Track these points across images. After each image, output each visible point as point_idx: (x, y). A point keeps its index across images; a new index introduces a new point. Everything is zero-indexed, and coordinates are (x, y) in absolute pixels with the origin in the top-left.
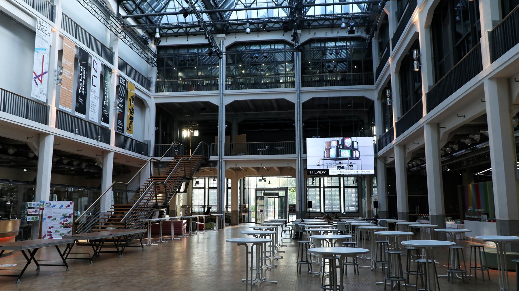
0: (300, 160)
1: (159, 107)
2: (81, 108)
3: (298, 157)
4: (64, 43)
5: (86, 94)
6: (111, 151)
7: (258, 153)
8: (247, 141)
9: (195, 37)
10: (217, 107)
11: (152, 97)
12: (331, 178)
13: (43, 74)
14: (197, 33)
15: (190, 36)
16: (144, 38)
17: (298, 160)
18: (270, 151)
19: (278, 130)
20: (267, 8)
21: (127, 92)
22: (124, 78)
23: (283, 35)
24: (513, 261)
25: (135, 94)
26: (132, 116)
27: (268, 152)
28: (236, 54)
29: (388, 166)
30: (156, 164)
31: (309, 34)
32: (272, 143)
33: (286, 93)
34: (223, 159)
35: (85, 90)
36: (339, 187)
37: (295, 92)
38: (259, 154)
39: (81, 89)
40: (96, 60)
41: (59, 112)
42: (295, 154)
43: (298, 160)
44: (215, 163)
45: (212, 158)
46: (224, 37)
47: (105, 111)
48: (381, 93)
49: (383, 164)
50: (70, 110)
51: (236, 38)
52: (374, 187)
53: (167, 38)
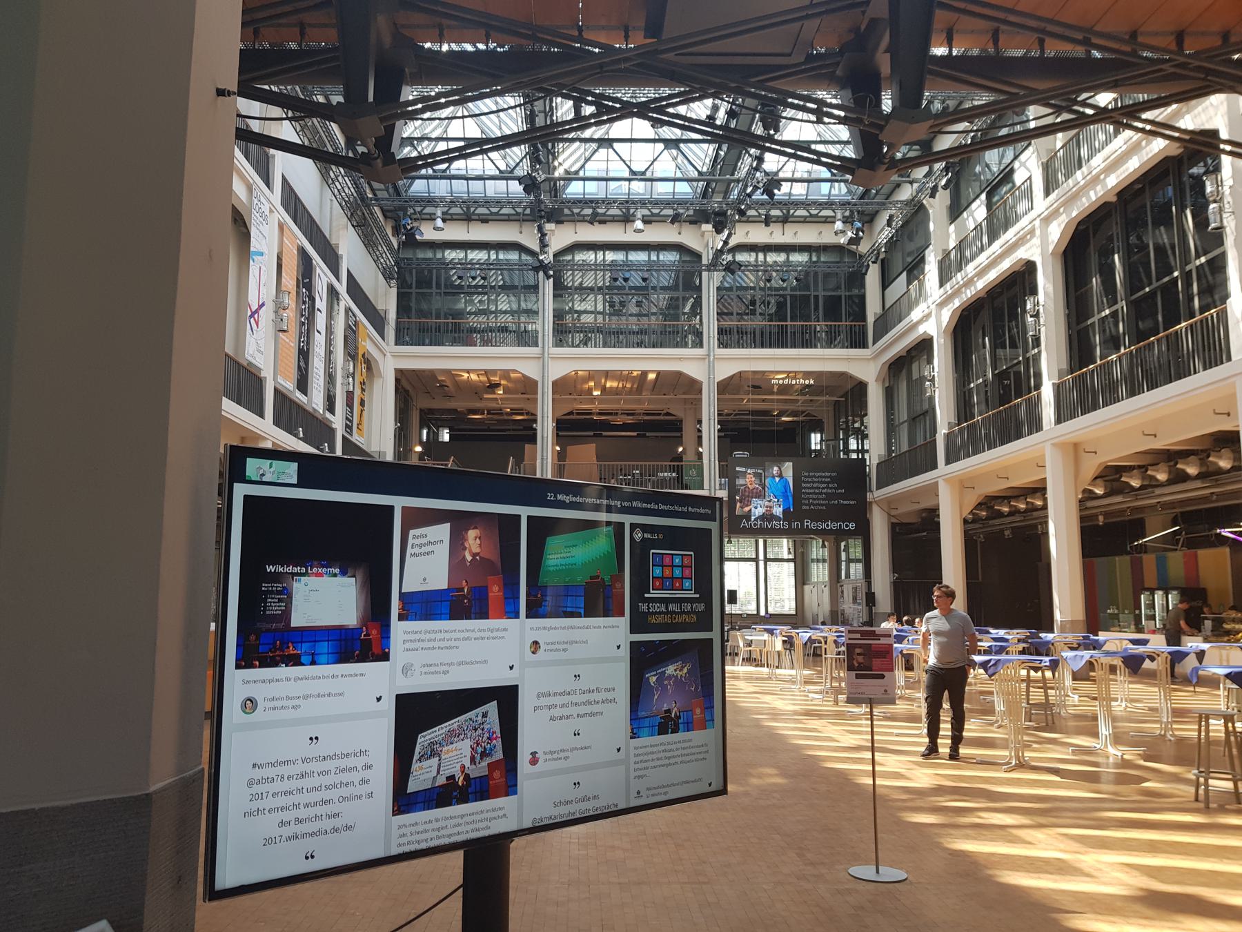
4: (285, 239)
5: (308, 349)
10: (536, 383)
11: (388, 354)
14: (490, 217)
16: (409, 227)
18: (642, 481)
19: (635, 434)
20: (809, 181)
21: (356, 348)
22: (354, 315)
23: (680, 233)
28: (415, 268)
29: (894, 520)
35: (308, 343)
36: (756, 560)
40: (322, 274)
41: (278, 393)
50: (289, 385)
52: (853, 562)
53: (681, 225)
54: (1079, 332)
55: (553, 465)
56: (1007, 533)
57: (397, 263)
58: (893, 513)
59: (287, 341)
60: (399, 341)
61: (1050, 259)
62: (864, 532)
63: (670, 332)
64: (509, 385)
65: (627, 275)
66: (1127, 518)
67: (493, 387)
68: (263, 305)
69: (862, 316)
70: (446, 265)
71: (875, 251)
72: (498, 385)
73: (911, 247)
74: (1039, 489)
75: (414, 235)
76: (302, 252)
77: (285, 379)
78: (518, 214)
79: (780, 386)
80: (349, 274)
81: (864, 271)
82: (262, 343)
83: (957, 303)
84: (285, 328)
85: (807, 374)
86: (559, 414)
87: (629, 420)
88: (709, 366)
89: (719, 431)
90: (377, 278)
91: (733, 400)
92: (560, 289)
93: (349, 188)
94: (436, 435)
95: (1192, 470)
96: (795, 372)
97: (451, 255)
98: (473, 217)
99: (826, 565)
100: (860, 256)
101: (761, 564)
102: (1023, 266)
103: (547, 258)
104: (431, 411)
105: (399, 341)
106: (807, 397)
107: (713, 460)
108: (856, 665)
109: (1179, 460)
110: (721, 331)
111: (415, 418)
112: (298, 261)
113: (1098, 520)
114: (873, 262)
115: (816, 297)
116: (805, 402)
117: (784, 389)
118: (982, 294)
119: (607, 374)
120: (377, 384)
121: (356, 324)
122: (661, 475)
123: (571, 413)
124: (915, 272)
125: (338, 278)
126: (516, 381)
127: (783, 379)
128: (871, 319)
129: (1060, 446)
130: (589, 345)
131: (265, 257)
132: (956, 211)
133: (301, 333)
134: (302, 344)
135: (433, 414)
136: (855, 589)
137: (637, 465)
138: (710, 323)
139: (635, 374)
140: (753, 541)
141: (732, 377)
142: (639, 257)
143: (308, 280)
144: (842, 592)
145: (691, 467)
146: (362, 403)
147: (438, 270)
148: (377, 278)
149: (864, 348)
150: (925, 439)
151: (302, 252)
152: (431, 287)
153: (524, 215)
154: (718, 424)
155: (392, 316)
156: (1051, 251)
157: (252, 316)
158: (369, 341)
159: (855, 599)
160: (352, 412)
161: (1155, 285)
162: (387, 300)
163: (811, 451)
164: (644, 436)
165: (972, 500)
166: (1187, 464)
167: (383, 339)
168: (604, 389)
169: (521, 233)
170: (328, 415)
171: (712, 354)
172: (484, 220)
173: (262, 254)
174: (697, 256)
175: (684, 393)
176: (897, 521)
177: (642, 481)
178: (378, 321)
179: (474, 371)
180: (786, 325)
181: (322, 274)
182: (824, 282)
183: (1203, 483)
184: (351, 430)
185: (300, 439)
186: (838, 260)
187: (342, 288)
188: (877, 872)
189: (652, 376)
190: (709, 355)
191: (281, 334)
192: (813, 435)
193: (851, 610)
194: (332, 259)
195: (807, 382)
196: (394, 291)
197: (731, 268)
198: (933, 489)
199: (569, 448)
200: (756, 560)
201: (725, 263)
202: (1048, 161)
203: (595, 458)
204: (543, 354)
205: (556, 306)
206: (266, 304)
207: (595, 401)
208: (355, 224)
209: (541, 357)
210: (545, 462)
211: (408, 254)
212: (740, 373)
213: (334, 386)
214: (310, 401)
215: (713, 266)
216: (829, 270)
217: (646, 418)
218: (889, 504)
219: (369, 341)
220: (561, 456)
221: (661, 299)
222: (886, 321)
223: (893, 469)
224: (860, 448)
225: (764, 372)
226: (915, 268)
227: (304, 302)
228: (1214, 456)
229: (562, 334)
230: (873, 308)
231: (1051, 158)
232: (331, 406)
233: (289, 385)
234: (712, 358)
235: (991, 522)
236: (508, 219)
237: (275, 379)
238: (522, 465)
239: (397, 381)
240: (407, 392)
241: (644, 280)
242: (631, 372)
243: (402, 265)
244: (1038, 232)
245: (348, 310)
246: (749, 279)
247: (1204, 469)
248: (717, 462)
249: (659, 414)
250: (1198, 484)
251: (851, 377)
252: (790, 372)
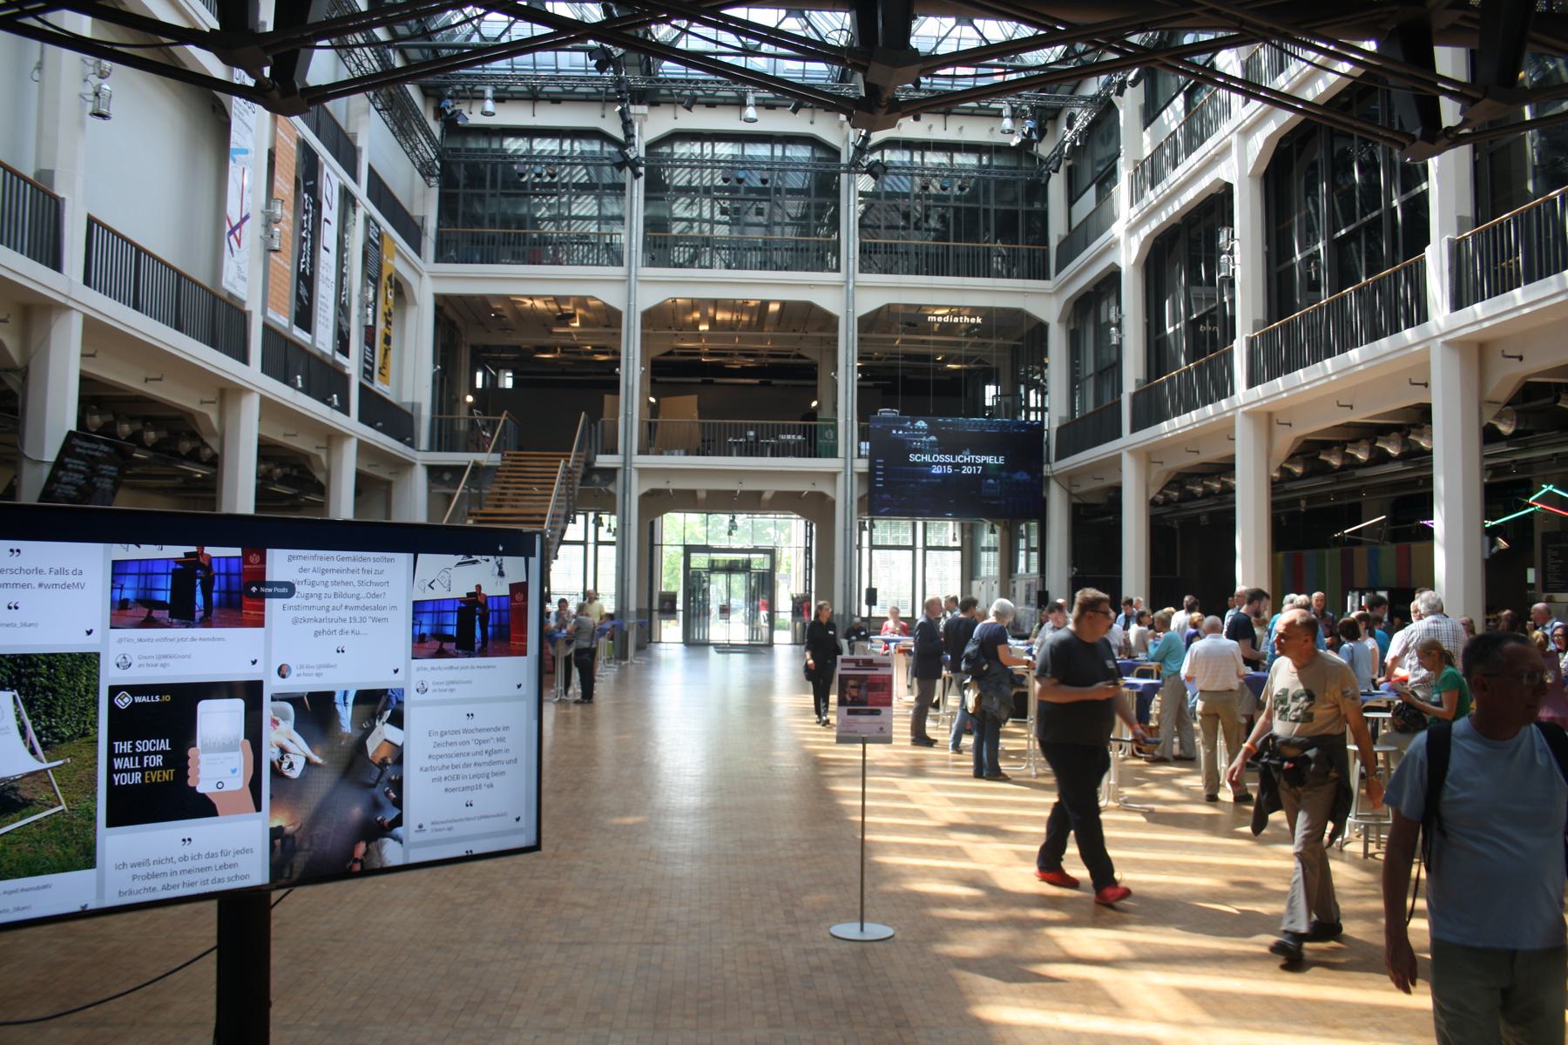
0: (852, 475)
1: (444, 305)
2: (304, 317)
3: (846, 468)
4: (278, 130)
5: (312, 273)
6: (350, 436)
7: (726, 451)
8: (700, 418)
9: (556, 107)
11: (426, 275)
13: (243, 220)
15: (541, 102)
16: (449, 112)
17: (846, 475)
18: (757, 448)
19: (757, 381)
21: (380, 266)
23: (812, 123)
25: (397, 271)
26: (388, 332)
27: (757, 450)
28: (463, 162)
29: (1076, 500)
30: (434, 472)
32: (773, 425)
33: (810, 285)
35: (312, 265)
36: (913, 548)
37: (842, 286)
38: (763, 455)
39: (303, 260)
40: (332, 175)
41: (269, 330)
42: (836, 457)
43: (846, 475)
44: (610, 473)
45: (603, 461)
46: (644, 115)
47: (343, 319)
48: (1071, 304)
49: (1066, 494)
50: (283, 320)
51: (676, 118)
54: (1279, 275)
55: (641, 422)
56: (1204, 518)
57: (439, 157)
58: (1075, 490)
59: (282, 262)
60: (440, 257)
61: (1248, 181)
62: (1038, 512)
63: (802, 250)
64: (588, 315)
65: (741, 175)
66: (1332, 504)
67: (566, 318)
68: (247, 217)
69: (1044, 240)
70: (508, 159)
71: (1058, 156)
72: (573, 316)
73: (1101, 152)
74: (1227, 467)
75: (456, 121)
76: (304, 147)
77: (279, 311)
78: (599, 93)
79: (942, 323)
80: (371, 170)
81: (1043, 181)
82: (245, 268)
83: (1154, 224)
84: (277, 247)
85: (975, 311)
86: (656, 352)
87: (750, 363)
88: (848, 297)
89: (859, 380)
90: (413, 175)
91: (884, 340)
92: (656, 189)
93: (369, 61)
94: (495, 380)
95: (1393, 450)
96: (959, 307)
97: (513, 145)
98: (541, 96)
99: (997, 554)
100: (1041, 160)
101: (919, 553)
102: (1221, 188)
103: (638, 150)
104: (487, 348)
105: (440, 257)
106: (976, 339)
107: (849, 419)
108: (849, 699)
109: (1379, 437)
110: (863, 250)
111: (465, 357)
112: (298, 156)
113: (1299, 506)
114: (1054, 171)
115: (986, 211)
116: (974, 345)
117: (947, 328)
118: (1176, 220)
119: (717, 304)
120: (411, 314)
121: (380, 236)
122: (783, 437)
123: (670, 353)
124: (1107, 184)
125: (354, 177)
126: (597, 310)
127: (943, 316)
128: (1053, 243)
129: (1252, 415)
131: (251, 156)
132: (1150, 113)
133: (301, 251)
134: (302, 266)
135: (490, 352)
136: (1029, 586)
137: (752, 425)
138: (850, 239)
139: (752, 303)
140: (910, 522)
141: (879, 311)
142: (762, 151)
143: (311, 183)
144: (1014, 590)
145: (827, 427)
146: (387, 340)
147: (494, 166)
148: (413, 175)
149: (1044, 279)
150: (1113, 399)
151: (304, 147)
152: (484, 187)
153: (607, 93)
154: (859, 372)
155: (431, 225)
156: (1249, 172)
157: (232, 232)
158: (399, 258)
159: (1028, 599)
160: (373, 352)
161: (1359, 222)
162: (425, 205)
163: (985, 408)
164: (769, 384)
165: (1160, 475)
166: (1388, 442)
167: (419, 254)
168: (713, 322)
169: (603, 116)
170: (339, 358)
171: (851, 281)
172: (555, 100)
173: (246, 152)
174: (834, 152)
175: (820, 330)
176: (1080, 501)
177: (757, 448)
178: (411, 230)
179: (538, 297)
180: (948, 247)
181: (332, 175)
182: (997, 193)
183: (1508, 446)
184: (372, 377)
185: (299, 390)
186: (1015, 164)
187: (360, 191)
188: (862, 929)
189: (774, 307)
190: (847, 282)
191: (272, 255)
192: (987, 387)
193: (1023, 613)
194: (347, 153)
195: (973, 320)
196: (435, 192)
197: (876, 170)
198: (1115, 462)
199: (662, 400)
200: (913, 548)
201: (865, 164)
202: (1248, 60)
203: (696, 415)
204: (629, 275)
205: (651, 211)
206: (251, 215)
207: (701, 337)
208: (379, 106)
209: (626, 281)
210: (629, 419)
211: (456, 143)
212: (889, 306)
213: (348, 319)
214: (314, 340)
215: (854, 167)
216: (1002, 177)
217: (772, 360)
218: (1069, 479)
219: (399, 258)
220: (655, 410)
221: (794, 207)
222: (1078, 239)
223: (1079, 434)
224: (1039, 405)
225: (920, 307)
226: (1107, 178)
227: (306, 212)
228: (1324, 454)
229: (660, 246)
230: (1057, 229)
231: (1251, 57)
232: (343, 346)
233: (283, 320)
234: (851, 286)
235: (1184, 505)
236: (587, 99)
237: (264, 312)
238: (599, 424)
239: (438, 309)
240: (452, 323)
241: (764, 181)
242: (746, 302)
243: (446, 158)
244: (1234, 150)
245: (368, 219)
246: (904, 185)
247: (1406, 450)
248: (855, 422)
249: (788, 357)
250: (1398, 467)
251: (1029, 317)
252: (952, 307)
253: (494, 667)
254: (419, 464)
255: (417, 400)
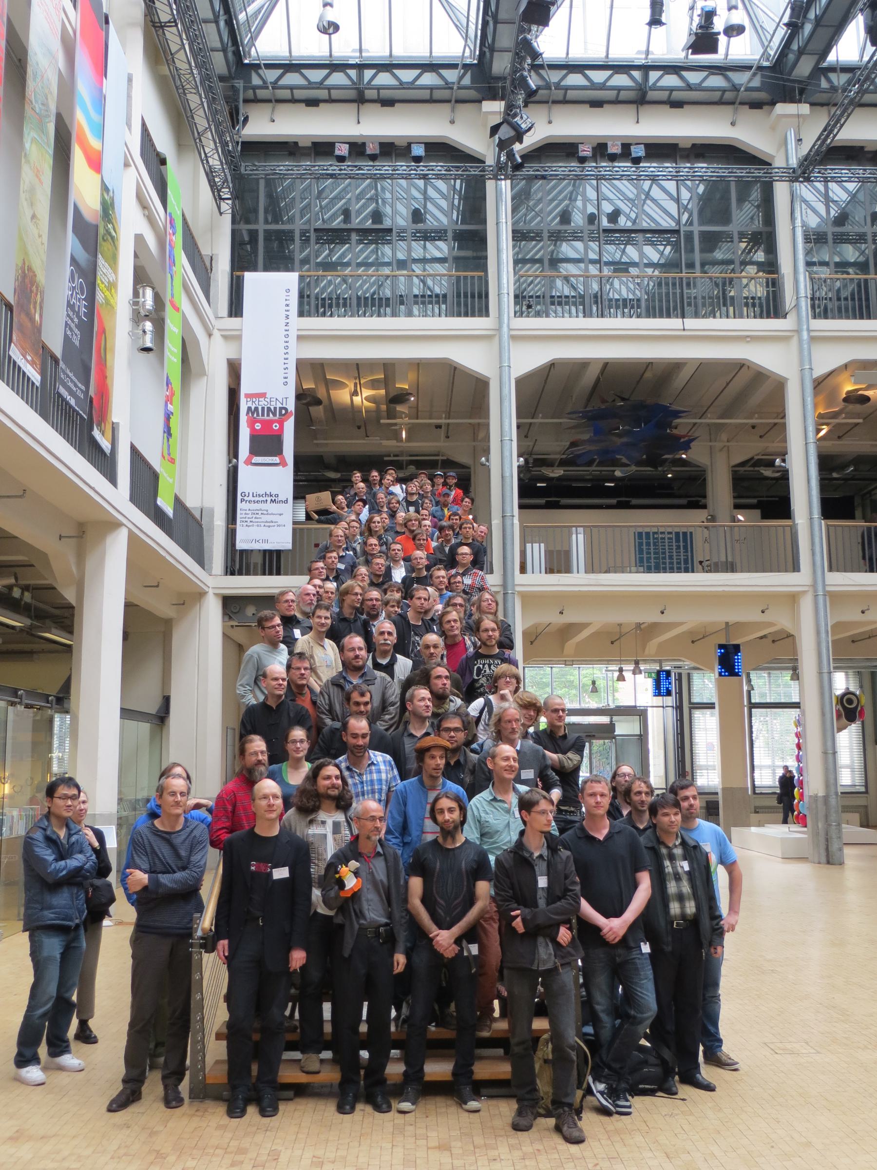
11: (217, 334)
12: (769, 674)
24: (649, 1045)
31: (359, 122)
34: (518, 589)
51: (550, 122)
53: (550, 109)
120: (198, 390)
130: (718, 314)
169: (452, 122)
170: (783, 464)
234: (805, 335)
253: (655, 21)
254: (211, 592)
255: (207, 504)
